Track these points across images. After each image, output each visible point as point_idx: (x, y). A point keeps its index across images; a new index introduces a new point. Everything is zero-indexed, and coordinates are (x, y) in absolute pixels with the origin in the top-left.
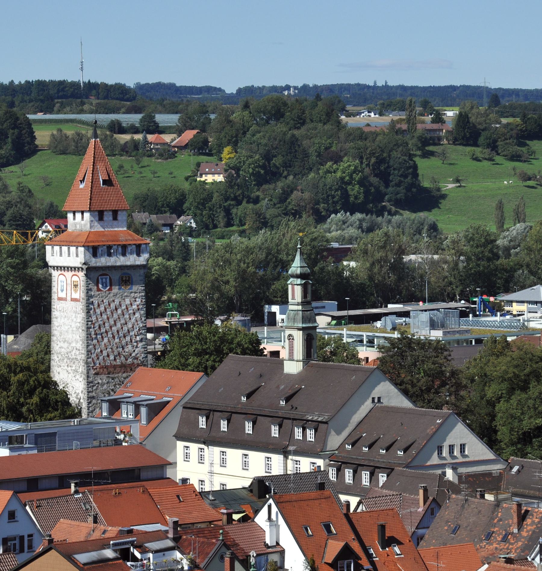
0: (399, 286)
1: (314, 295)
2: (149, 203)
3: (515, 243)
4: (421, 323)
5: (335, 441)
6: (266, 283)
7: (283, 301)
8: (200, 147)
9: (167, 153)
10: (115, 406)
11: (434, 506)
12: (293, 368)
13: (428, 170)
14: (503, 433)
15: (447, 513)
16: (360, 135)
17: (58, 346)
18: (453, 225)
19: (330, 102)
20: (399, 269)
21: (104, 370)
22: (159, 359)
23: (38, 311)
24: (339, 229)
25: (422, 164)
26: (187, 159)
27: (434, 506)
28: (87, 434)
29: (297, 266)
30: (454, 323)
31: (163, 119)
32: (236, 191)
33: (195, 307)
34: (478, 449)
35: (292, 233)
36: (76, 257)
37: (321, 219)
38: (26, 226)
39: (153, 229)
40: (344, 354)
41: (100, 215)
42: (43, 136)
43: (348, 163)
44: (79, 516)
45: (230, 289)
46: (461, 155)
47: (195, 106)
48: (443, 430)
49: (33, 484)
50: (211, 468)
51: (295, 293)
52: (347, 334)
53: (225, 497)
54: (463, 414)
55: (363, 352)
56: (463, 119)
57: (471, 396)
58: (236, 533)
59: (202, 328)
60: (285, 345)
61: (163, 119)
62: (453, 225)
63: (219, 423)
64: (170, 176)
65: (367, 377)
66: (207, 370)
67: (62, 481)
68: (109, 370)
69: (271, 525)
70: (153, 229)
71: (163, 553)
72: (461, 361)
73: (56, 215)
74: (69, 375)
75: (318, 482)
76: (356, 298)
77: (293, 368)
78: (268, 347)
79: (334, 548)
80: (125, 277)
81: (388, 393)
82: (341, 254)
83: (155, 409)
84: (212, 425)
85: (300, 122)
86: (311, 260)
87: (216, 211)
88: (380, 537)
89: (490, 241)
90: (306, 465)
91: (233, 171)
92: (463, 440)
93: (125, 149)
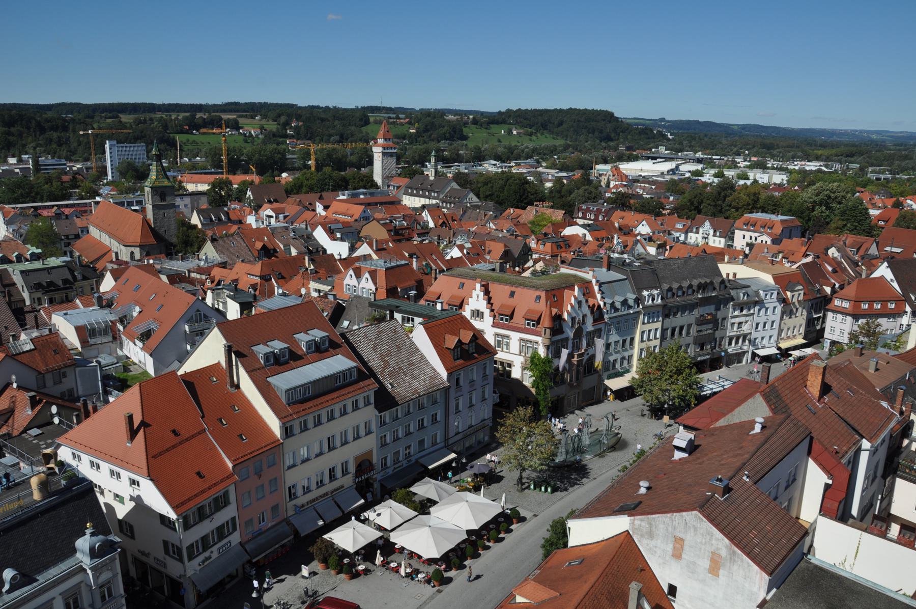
0: (458, 159)
1: (437, 161)
2: (397, 137)
3: (486, 149)
4: (463, 168)
5: (441, 196)
6: (425, 157)
7: (430, 162)
8: (410, 123)
9: (402, 124)
10: (389, 186)
11: (465, 212)
12: (432, 178)
13: (465, 131)
14: (481, 196)
15: (467, 214)
16: (449, 121)
17: (375, 171)
18: (471, 144)
19: (442, 113)
20: (458, 155)
21: (387, 178)
22: (399, 175)
23: (370, 162)
24: (443, 144)
25: (464, 129)
26: (407, 126)
27: (465, 212)
28: (382, 193)
29: (433, 153)
30: (471, 169)
31: (401, 116)
32: (418, 134)
33: (408, 163)
34: (475, 199)
35: (433, 145)
36: (380, 149)
37: (439, 142)
38: (368, 142)
39: (398, 143)
40: (444, 175)
41: (386, 140)
42: (371, 120)
43: (446, 128)
44: (381, 212)
45: (417, 158)
46: (473, 127)
47: (408, 112)
48: (468, 194)
49: (369, 204)
50: (411, 202)
51: (433, 160)
52: (445, 170)
53: (415, 209)
54: (472, 191)
55: (449, 175)
56: (474, 118)
57: (474, 186)
58: (418, 218)
59: (409, 167)
60: (430, 172)
61: (401, 116)
62: (471, 144)
63: (414, 191)
64: (401, 130)
65: (449, 181)
66: (411, 178)
67: (376, 204)
68: (387, 177)
69: (426, 215)
70: (398, 143)
71: (509, 289)
72: (472, 178)
73: (375, 140)
74: (378, 178)
75: (437, 206)
76: (447, 161)
77: (432, 178)
78: (426, 173)
79: (441, 222)
80: (391, 155)
81: (454, 185)
82: (444, 151)
83: (398, 187)
84: (412, 191)
85: (435, 118)
86: (436, 152)
87: (413, 139)
88: (869, 585)
89: (480, 149)
90: (434, 202)
91: (418, 129)
92: (472, 198)
93: (392, 123)
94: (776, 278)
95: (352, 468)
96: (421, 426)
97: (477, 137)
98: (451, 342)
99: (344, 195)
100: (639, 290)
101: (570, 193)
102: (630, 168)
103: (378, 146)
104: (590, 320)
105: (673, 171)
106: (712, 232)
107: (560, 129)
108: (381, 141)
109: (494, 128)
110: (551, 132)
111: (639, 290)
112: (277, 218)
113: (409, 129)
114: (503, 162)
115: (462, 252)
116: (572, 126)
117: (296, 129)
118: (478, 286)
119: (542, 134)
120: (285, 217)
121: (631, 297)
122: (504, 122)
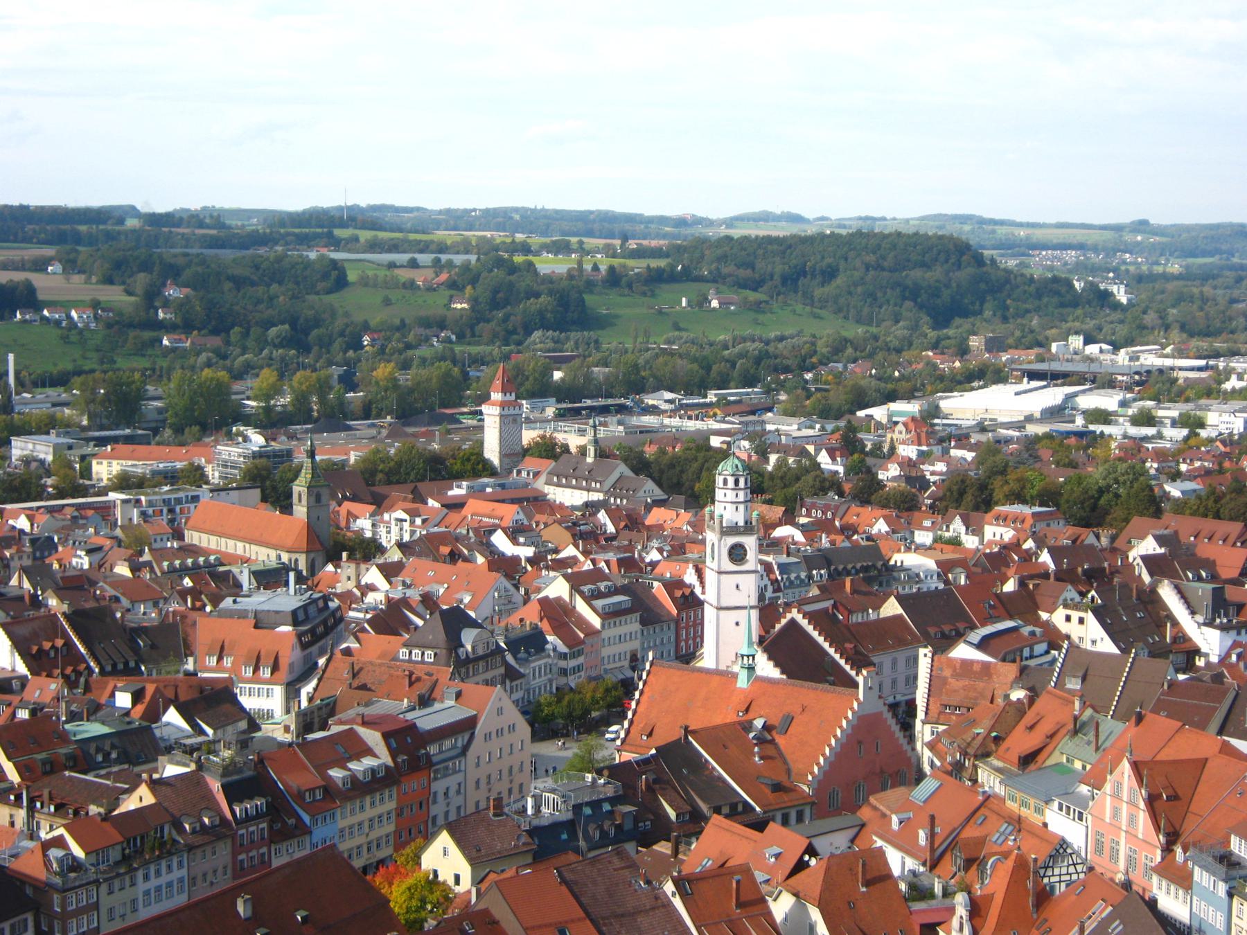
16: (549, 279)
25: (586, 297)
32: (477, 316)
36: (496, 410)
79: (622, 524)
91: (474, 301)
94: (938, 563)
95: (628, 657)
96: (662, 643)
97: (631, 335)
98: (678, 593)
99: (459, 487)
100: (810, 570)
101: (798, 479)
102: (962, 407)
103: (494, 404)
104: (770, 589)
105: (1053, 413)
106: (963, 529)
107: (829, 289)
108: (496, 396)
109: (665, 292)
110: (809, 299)
111: (810, 570)
112: (412, 523)
113: (451, 299)
114: (689, 393)
115: (661, 553)
116: (862, 281)
117: (182, 305)
118: (691, 566)
119: (786, 303)
120: (424, 521)
121: (803, 575)
122: (687, 276)
